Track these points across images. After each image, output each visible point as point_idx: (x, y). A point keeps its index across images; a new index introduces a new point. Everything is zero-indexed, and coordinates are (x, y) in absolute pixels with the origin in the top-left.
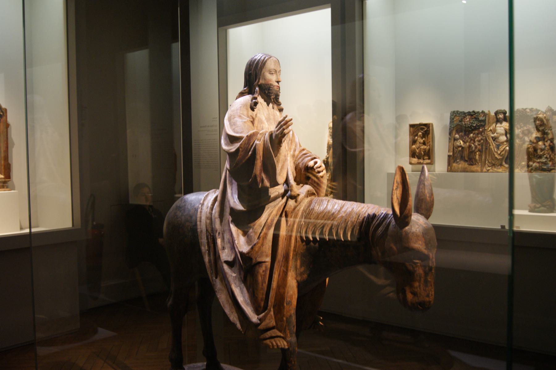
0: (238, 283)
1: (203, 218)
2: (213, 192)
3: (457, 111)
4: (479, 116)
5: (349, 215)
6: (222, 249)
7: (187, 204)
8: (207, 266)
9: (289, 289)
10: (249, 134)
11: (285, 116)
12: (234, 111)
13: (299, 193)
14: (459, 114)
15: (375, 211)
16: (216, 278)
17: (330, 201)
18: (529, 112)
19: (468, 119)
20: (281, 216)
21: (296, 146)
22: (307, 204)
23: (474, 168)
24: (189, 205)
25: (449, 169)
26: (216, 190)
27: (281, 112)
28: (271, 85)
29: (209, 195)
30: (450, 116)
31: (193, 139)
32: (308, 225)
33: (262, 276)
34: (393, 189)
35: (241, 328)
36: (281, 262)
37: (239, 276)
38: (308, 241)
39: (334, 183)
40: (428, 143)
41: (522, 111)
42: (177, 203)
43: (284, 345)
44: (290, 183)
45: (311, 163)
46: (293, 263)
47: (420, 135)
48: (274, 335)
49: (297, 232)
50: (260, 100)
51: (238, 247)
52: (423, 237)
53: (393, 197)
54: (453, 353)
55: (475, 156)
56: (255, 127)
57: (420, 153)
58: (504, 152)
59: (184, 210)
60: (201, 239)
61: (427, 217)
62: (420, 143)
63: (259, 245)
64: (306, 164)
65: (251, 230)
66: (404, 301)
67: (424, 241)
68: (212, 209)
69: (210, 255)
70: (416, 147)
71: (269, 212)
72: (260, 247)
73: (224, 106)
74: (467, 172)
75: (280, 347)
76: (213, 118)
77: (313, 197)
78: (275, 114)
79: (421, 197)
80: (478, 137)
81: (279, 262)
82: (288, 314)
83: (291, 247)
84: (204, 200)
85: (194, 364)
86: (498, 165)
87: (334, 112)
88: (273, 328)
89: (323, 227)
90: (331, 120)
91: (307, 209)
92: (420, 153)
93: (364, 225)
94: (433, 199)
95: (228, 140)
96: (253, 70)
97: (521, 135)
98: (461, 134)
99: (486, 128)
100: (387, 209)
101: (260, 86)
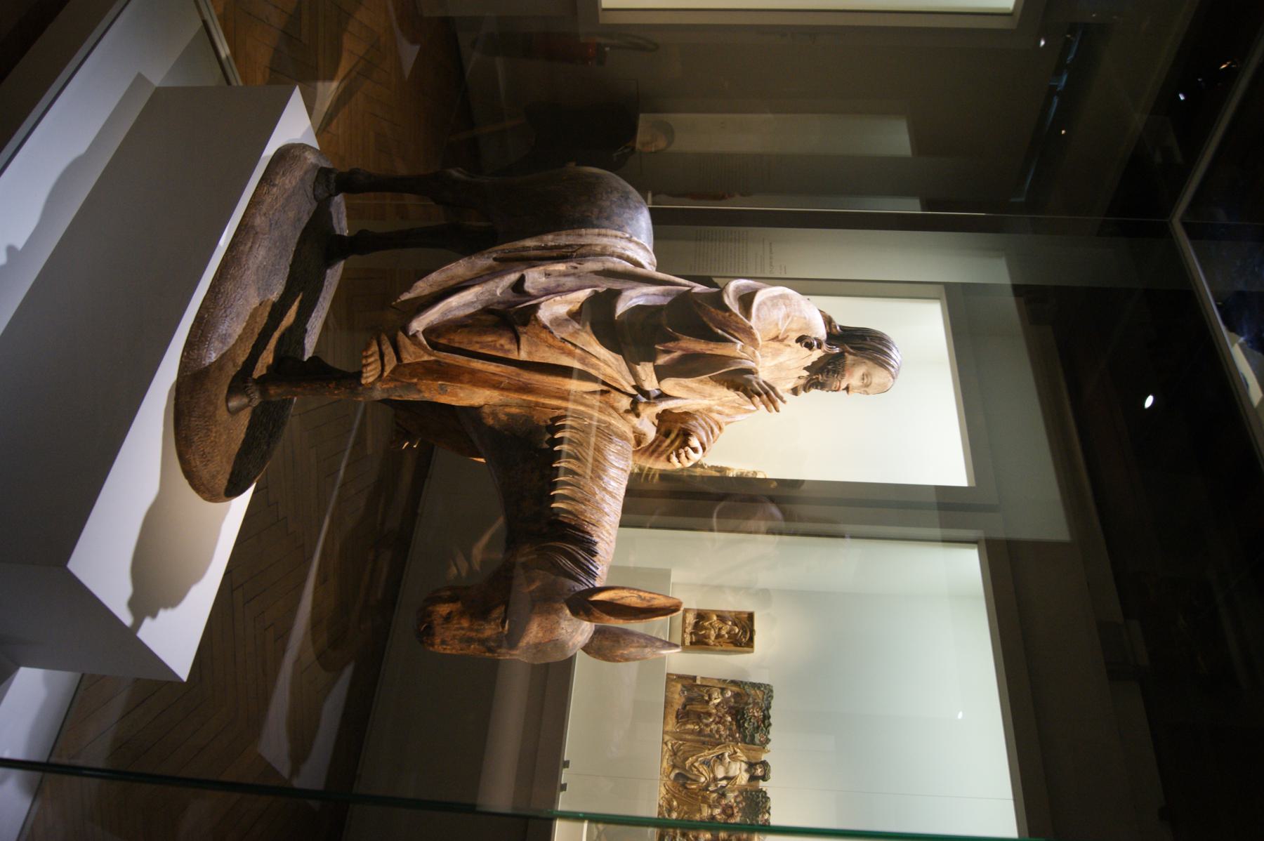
0: (482, 297)
1: (605, 241)
2: (651, 260)
3: (771, 697)
5: (597, 506)
6: (547, 272)
7: (631, 212)
8: (517, 242)
9: (467, 391)
10: (755, 331)
11: (784, 399)
12: (799, 305)
13: (641, 418)
15: (602, 555)
16: (495, 259)
17: (625, 474)
18: (763, 817)
20: (604, 383)
21: (727, 415)
22: (621, 432)
23: (672, 720)
24: (630, 216)
25: (671, 677)
26: (654, 266)
27: (791, 391)
28: (843, 376)
29: (646, 253)
30: (764, 684)
31: (748, 228)
32: (583, 432)
33: (493, 344)
34: (639, 590)
35: (402, 301)
36: (517, 379)
37: (495, 300)
38: (553, 429)
39: (657, 476)
40: (719, 642)
41: (766, 807)
42: (635, 194)
43: (367, 377)
44: (661, 402)
45: (694, 442)
46: (516, 401)
47: (734, 630)
48: (386, 359)
49: (575, 411)
50: (817, 354)
51: (549, 301)
52: (550, 641)
53: (625, 591)
54: (348, 672)
55: (693, 723)
56: (766, 343)
58: (696, 773)
59: (621, 206)
60: (567, 235)
61: (586, 649)
62: (720, 629)
63: (550, 340)
64: (694, 432)
65: (577, 326)
66: (436, 599)
67: (543, 642)
68: (621, 257)
69: (537, 250)
71: (610, 360)
72: (546, 342)
73: (809, 287)
74: (665, 707)
75: (364, 371)
76: (785, 267)
77: (633, 442)
78: (789, 381)
79: (624, 639)
80: (725, 730)
81: (518, 375)
82: (423, 387)
83: (544, 397)
84: (637, 243)
85: (345, 214)
86: (675, 761)
87: (782, 482)
88: (399, 359)
89: (577, 459)
90: (770, 475)
91: (613, 431)
93: (577, 533)
94: (618, 661)
95: (746, 292)
96: (872, 343)
97: (724, 802)
98: (733, 700)
99: (739, 744)
100: (605, 577)
101: (841, 355)
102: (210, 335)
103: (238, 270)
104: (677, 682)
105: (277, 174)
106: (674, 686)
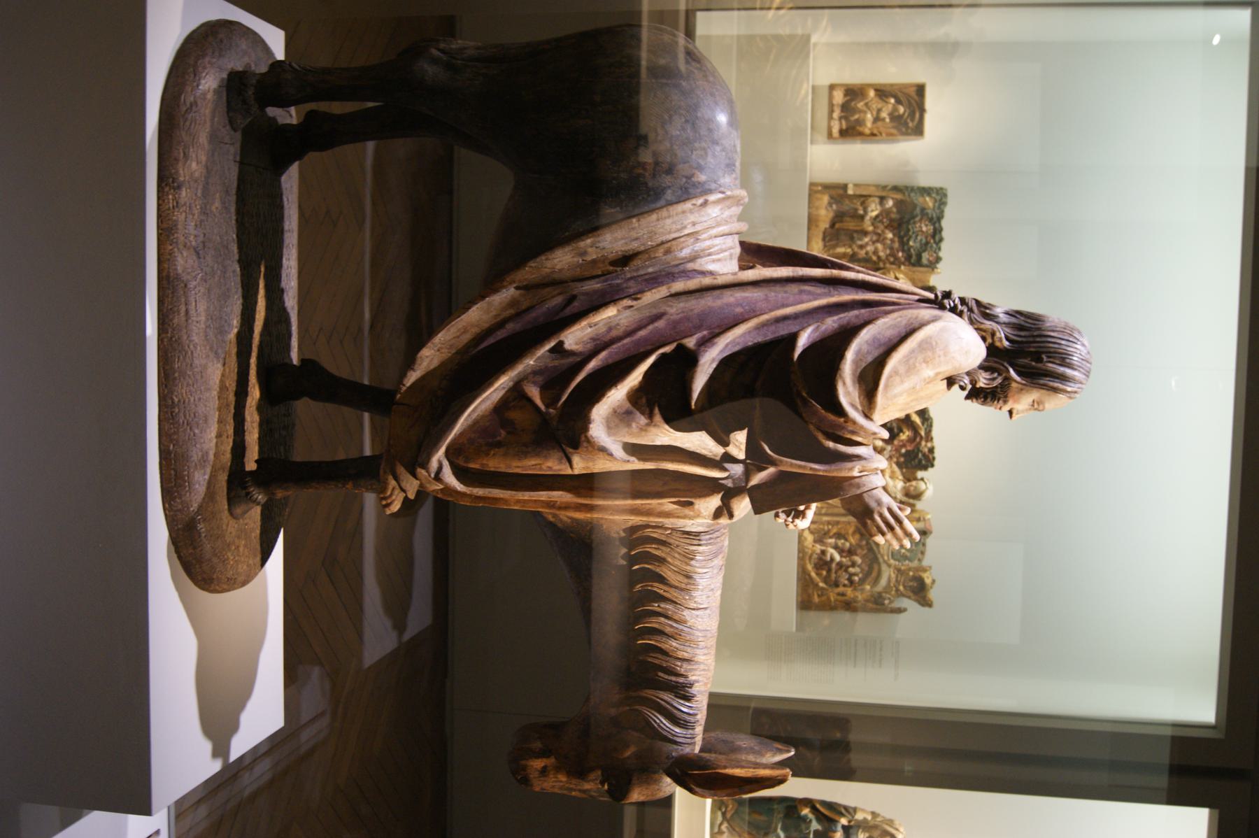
4: (931, 250)
14: (939, 208)
16: (517, 288)
19: (926, 228)
25: (815, 188)
30: (936, 188)
55: (844, 245)
57: (855, 110)
62: (879, 111)
70: (871, 101)
74: (809, 229)
80: (885, 248)
92: (855, 110)
98: (894, 210)
99: (903, 267)
102: (186, 473)
103: (184, 358)
104: (824, 193)
105: (177, 160)
106: (818, 199)
